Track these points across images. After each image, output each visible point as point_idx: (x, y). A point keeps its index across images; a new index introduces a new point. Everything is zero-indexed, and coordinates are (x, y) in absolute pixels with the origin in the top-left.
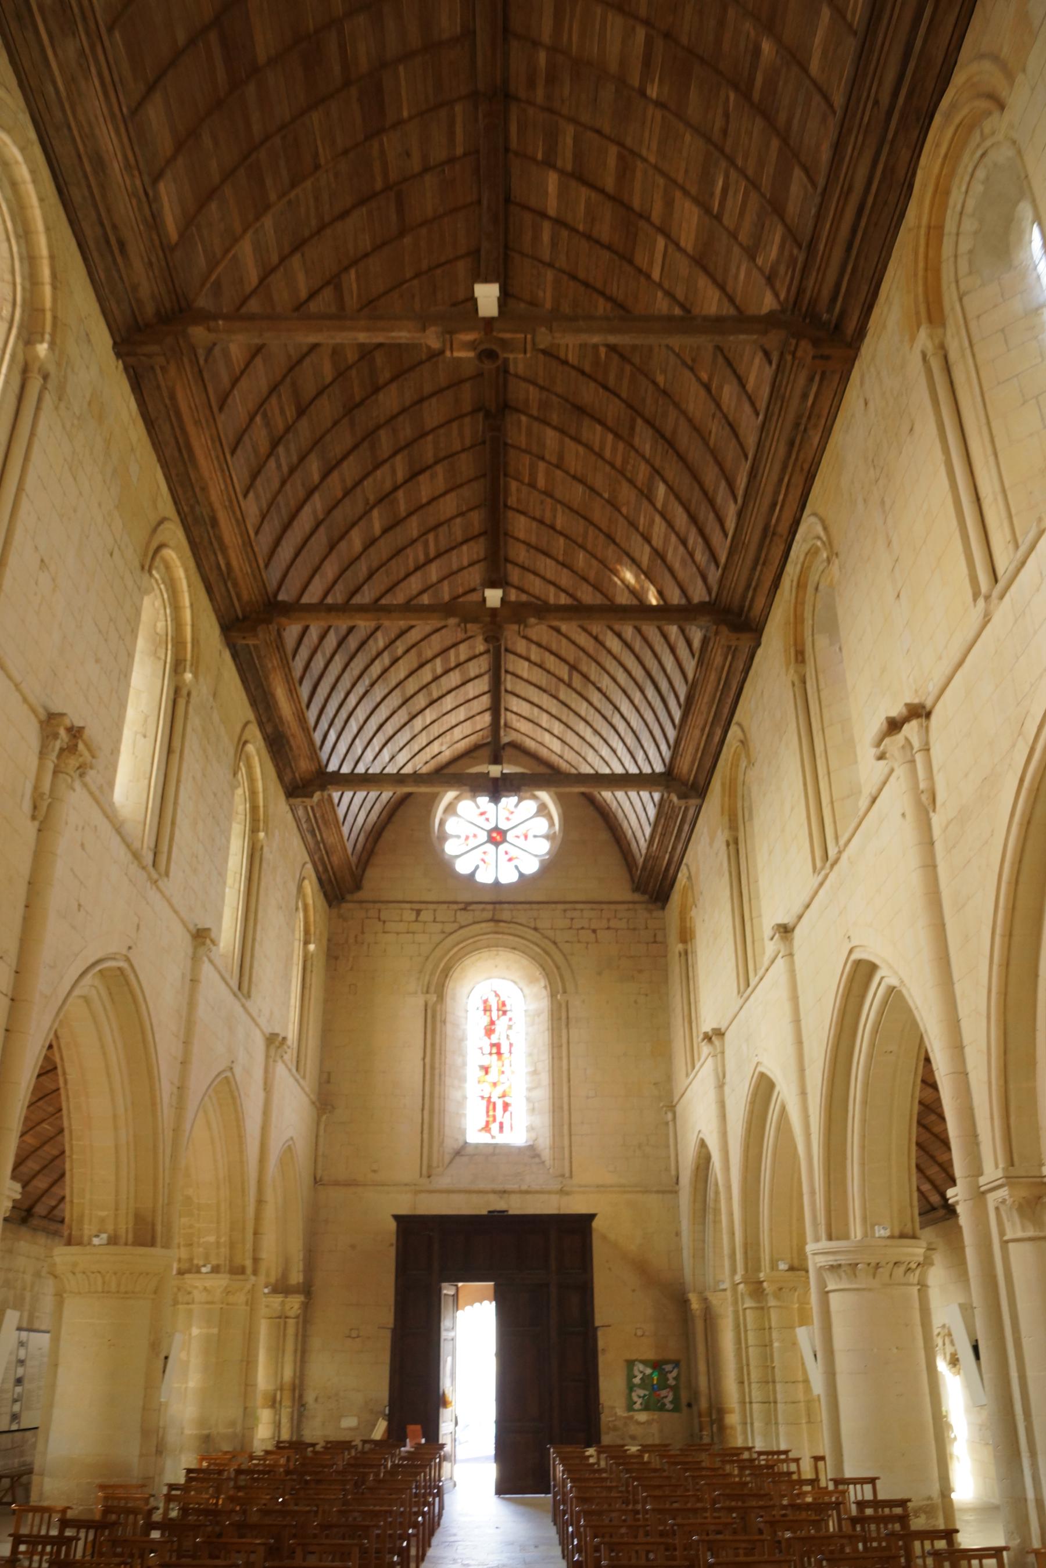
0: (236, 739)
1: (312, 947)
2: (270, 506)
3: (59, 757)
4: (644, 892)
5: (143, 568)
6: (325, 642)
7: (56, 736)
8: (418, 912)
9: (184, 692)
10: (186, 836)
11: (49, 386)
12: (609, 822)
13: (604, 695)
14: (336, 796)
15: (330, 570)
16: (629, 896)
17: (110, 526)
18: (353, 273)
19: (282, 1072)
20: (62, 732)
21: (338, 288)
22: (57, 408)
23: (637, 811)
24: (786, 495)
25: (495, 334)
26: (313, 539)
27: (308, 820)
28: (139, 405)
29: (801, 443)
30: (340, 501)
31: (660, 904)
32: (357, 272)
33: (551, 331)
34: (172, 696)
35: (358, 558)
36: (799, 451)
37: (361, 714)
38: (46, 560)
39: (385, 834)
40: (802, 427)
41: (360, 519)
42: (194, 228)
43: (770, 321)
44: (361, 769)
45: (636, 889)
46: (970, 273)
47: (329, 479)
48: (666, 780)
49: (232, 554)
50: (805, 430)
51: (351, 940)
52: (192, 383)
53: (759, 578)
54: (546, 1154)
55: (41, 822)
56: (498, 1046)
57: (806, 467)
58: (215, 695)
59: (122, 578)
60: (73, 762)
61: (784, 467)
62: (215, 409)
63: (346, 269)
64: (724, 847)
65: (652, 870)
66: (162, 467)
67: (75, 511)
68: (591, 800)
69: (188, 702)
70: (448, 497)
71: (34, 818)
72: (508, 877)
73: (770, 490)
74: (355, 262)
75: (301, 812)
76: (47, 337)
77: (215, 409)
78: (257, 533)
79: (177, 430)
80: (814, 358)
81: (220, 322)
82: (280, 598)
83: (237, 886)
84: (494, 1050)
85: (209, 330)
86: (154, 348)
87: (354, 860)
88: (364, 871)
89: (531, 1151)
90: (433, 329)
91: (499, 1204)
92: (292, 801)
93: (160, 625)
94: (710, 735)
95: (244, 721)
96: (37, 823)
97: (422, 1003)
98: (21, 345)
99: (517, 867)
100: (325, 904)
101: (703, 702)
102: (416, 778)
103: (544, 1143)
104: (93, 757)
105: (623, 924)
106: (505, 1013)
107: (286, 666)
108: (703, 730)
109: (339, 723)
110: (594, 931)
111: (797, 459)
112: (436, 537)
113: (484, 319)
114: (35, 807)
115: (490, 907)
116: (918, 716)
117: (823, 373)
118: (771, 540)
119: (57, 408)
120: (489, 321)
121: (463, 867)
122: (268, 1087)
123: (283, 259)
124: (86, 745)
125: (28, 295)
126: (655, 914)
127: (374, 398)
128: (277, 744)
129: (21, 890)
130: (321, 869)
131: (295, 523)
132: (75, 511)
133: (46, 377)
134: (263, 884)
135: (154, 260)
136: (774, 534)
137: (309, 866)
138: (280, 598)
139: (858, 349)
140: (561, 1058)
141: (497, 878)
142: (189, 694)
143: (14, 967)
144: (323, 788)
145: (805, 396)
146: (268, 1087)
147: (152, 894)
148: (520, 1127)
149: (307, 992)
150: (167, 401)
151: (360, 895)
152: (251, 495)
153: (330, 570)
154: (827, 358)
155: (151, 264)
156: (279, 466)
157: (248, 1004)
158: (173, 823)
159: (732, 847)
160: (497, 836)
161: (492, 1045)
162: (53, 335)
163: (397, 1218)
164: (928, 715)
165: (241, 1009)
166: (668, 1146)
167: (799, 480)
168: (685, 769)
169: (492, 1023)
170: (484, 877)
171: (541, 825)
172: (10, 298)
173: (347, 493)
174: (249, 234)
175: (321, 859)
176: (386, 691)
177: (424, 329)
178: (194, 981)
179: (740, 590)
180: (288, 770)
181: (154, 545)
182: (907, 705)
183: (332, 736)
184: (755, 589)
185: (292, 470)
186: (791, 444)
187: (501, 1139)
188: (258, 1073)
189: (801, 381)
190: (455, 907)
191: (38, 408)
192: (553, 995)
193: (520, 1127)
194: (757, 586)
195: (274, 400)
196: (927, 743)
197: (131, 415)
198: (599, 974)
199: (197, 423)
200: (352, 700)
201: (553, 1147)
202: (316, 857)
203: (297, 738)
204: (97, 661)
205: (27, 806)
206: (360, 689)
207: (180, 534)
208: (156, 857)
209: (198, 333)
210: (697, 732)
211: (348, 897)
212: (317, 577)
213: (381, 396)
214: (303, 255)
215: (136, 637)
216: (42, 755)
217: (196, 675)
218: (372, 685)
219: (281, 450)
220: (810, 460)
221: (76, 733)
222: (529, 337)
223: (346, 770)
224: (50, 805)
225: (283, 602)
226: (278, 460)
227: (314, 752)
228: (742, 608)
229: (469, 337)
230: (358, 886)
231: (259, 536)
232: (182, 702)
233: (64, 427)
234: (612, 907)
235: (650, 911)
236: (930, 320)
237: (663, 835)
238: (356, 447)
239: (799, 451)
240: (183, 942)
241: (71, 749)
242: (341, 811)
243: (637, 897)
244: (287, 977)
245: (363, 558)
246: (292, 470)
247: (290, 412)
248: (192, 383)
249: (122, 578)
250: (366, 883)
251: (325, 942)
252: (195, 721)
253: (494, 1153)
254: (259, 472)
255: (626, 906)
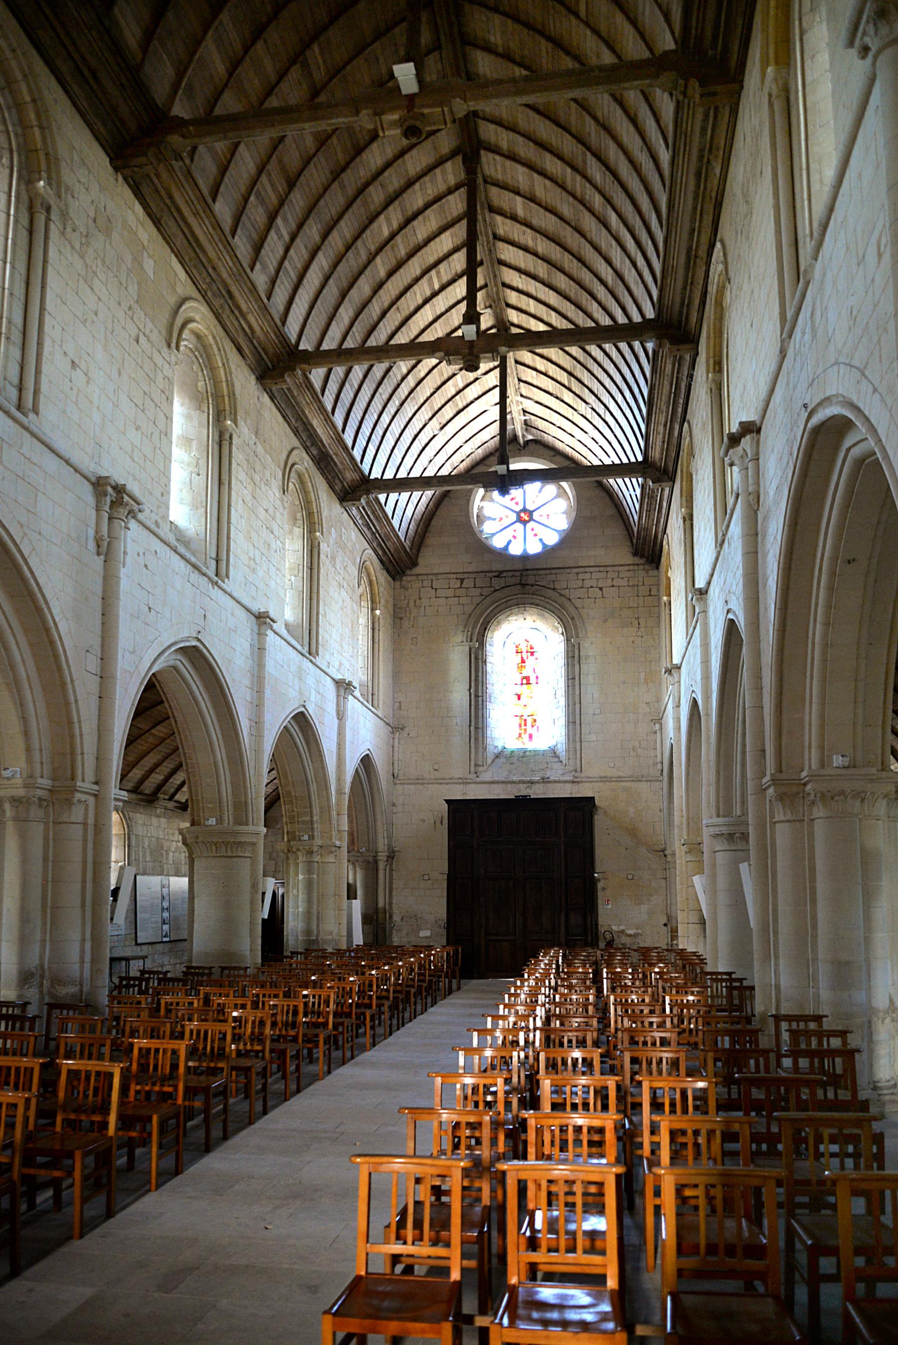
0: (282, 464)
1: (378, 612)
2: (278, 272)
3: (111, 508)
4: (642, 556)
5: (169, 346)
6: (351, 375)
7: (105, 494)
8: (462, 580)
9: (227, 436)
10: (240, 545)
11: (53, 217)
12: (613, 499)
13: (596, 396)
14: (382, 497)
15: (345, 314)
16: (629, 559)
17: (132, 319)
18: (315, 47)
19: (353, 705)
20: (110, 489)
21: (305, 65)
22: (63, 233)
23: (629, 489)
24: (700, 222)
25: (416, 110)
26: (325, 291)
27: (362, 516)
28: (144, 208)
29: (707, 172)
30: (343, 256)
31: (654, 565)
32: (320, 45)
33: (465, 101)
34: (217, 438)
35: (369, 300)
36: (706, 180)
37: (396, 428)
38: (77, 362)
39: (433, 522)
40: (705, 160)
41: (365, 267)
42: (156, 42)
43: (657, 65)
44: (402, 474)
45: (635, 554)
46: (811, 10)
47: (330, 238)
48: (641, 469)
49: (251, 318)
50: (709, 161)
51: (412, 605)
52: (184, 182)
53: (690, 297)
54: (563, 755)
55: (106, 555)
56: (528, 678)
57: (714, 195)
58: (256, 434)
59: (151, 358)
60: (122, 512)
61: (696, 198)
62: (210, 201)
63: (308, 46)
64: (681, 521)
65: (645, 538)
66: (176, 256)
67: (96, 314)
68: (600, 484)
69: (231, 443)
70: (443, 236)
71: (98, 554)
72: (534, 548)
73: (687, 218)
74: (314, 39)
75: (354, 511)
76: (44, 175)
77: (210, 201)
78: (269, 299)
79: (181, 223)
80: (702, 96)
81: (191, 128)
82: (301, 347)
83: (301, 574)
84: (525, 681)
85: (183, 137)
86: (142, 160)
87: (407, 545)
88: (418, 552)
89: (553, 752)
90: (364, 112)
91: (524, 791)
92: (345, 504)
93: (201, 384)
94: (672, 429)
95: (289, 448)
96: (102, 557)
97: (467, 648)
98: (23, 187)
99: (541, 540)
100: (389, 578)
101: (662, 404)
102: (448, 479)
103: (561, 748)
104: (138, 504)
105: (624, 582)
106: (532, 654)
107: (318, 401)
108: (665, 425)
109: (376, 439)
110: (601, 589)
111: (705, 188)
112: (438, 273)
113: (407, 96)
114: (99, 546)
115: (518, 574)
116: (750, 431)
117: (716, 108)
118: (695, 263)
119: (63, 233)
120: (411, 97)
121: (498, 543)
122: (341, 716)
123: (246, 50)
124: (130, 497)
125: (21, 140)
126: (651, 573)
127: (358, 159)
128: (323, 461)
129: (98, 603)
130: (380, 552)
131: (305, 281)
132: (96, 314)
133: (48, 210)
134: (322, 571)
135: (124, 81)
136: (696, 257)
137: (370, 551)
138: (301, 347)
139: (742, 81)
140: (574, 686)
141: (525, 550)
142: (231, 437)
143: (99, 655)
144: (368, 492)
145: (704, 129)
146: (341, 716)
147: (216, 593)
148: (550, 734)
149: (376, 645)
150: (167, 201)
151: (417, 570)
152: (258, 266)
153: (345, 314)
154: (714, 94)
155: (122, 84)
156: (280, 237)
157: (318, 661)
158: (228, 538)
159: (688, 522)
160: (525, 517)
161: (524, 678)
162: (49, 171)
163: (447, 801)
164: (759, 431)
165: (310, 664)
166: (655, 749)
167: (710, 207)
168: (657, 455)
169: (523, 661)
170: (516, 550)
171: (562, 505)
172: (6, 146)
173: (348, 248)
174: (210, 33)
175: (379, 545)
176: (416, 408)
177: (357, 113)
178: (261, 649)
179: (677, 307)
180: (337, 481)
181: (179, 322)
182: (741, 423)
183: (371, 450)
184: (688, 306)
185: (293, 238)
186: (698, 174)
187: (530, 746)
188: (331, 708)
189: (699, 116)
190: (491, 575)
191: (46, 238)
192: (568, 640)
193: (550, 734)
194: (689, 303)
195: (264, 179)
196: (757, 453)
197: (138, 219)
198: (605, 621)
199: (196, 214)
200: (386, 419)
201: (568, 751)
202: (375, 544)
203: (339, 458)
204: (138, 428)
205: (92, 545)
206: (391, 408)
207: (204, 309)
208: (214, 563)
209: (175, 139)
210: (661, 429)
211: (408, 572)
212: (334, 323)
213: (364, 155)
214: (265, 41)
215: (172, 403)
216: (98, 509)
217: (235, 421)
218: (402, 404)
219: (279, 221)
220: (715, 188)
221: (120, 490)
222: (446, 109)
223: (389, 475)
224: (109, 543)
225: (305, 351)
226: (278, 232)
227: (356, 468)
228: (680, 322)
229: (395, 117)
230: (415, 564)
231: (272, 299)
232: (226, 444)
233: (73, 247)
234: (617, 568)
235: (647, 571)
236: (777, 63)
237: (648, 511)
238: (349, 205)
239: (706, 180)
240: (246, 624)
241: (117, 503)
242: (389, 510)
243: (637, 560)
244: (354, 637)
245: (374, 300)
246: (293, 238)
247: (281, 187)
248: (184, 182)
249: (151, 358)
250: (421, 561)
251: (391, 608)
252: (238, 456)
253: (523, 757)
254: (262, 245)
255: (627, 568)
